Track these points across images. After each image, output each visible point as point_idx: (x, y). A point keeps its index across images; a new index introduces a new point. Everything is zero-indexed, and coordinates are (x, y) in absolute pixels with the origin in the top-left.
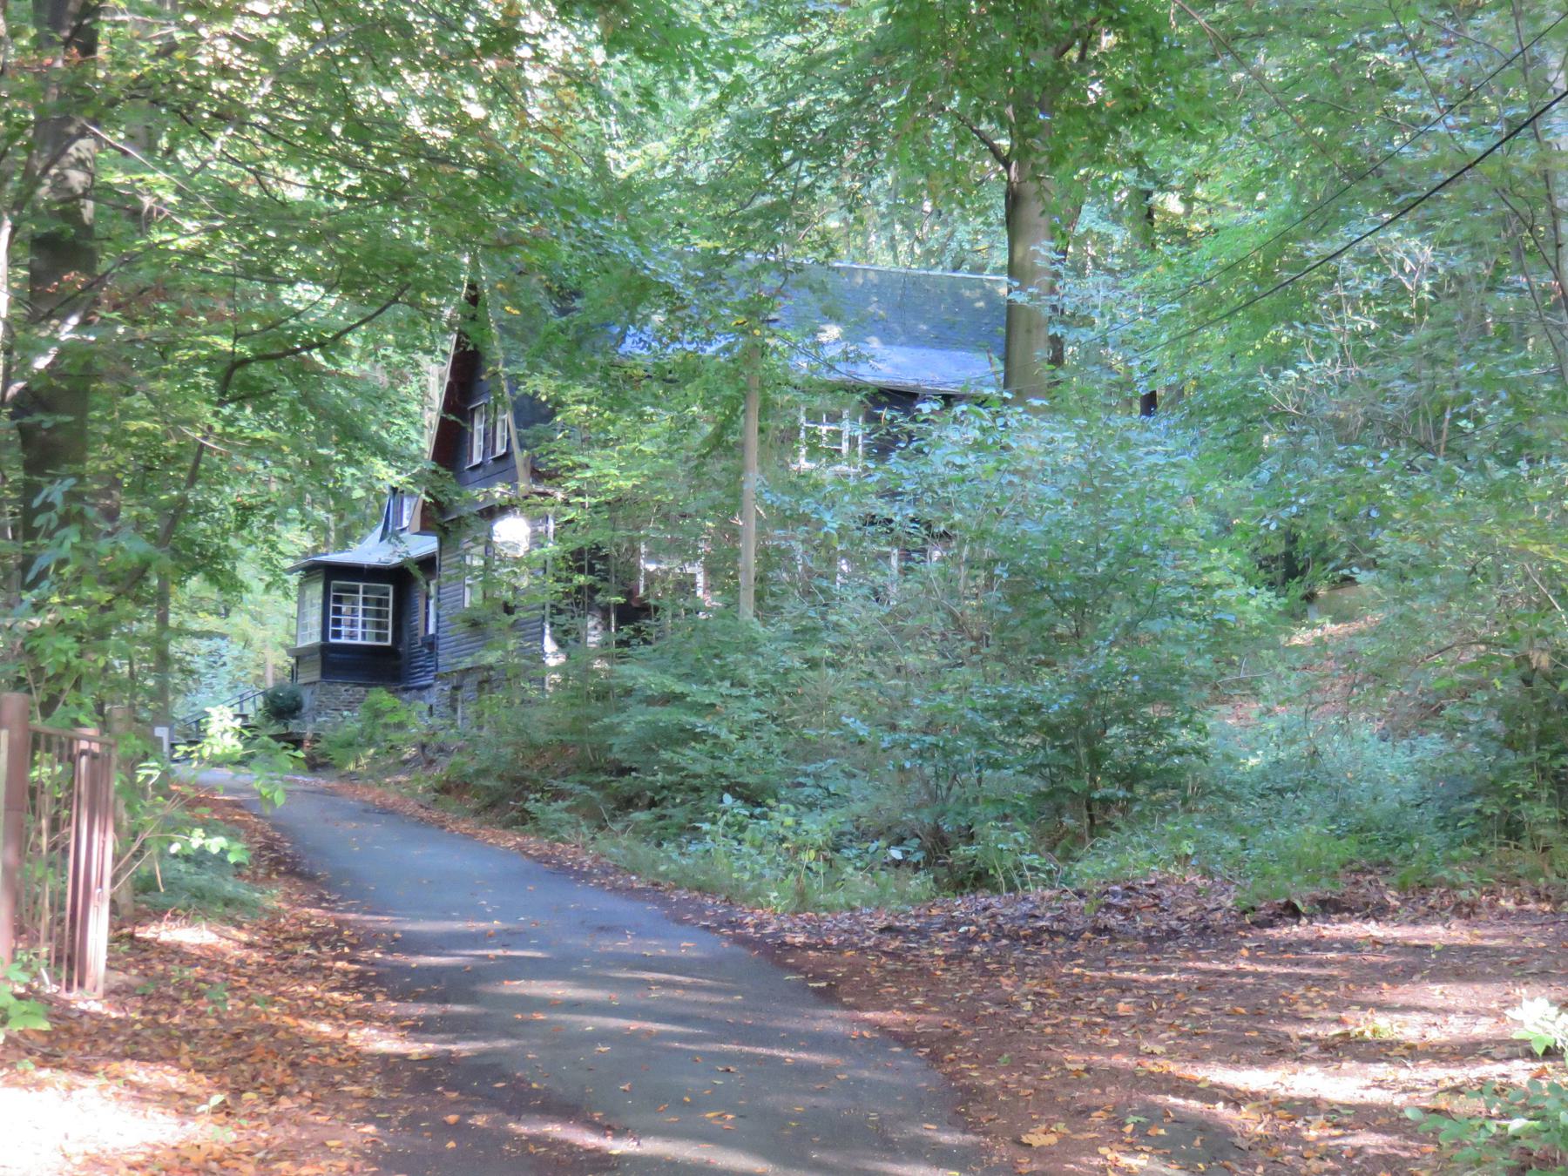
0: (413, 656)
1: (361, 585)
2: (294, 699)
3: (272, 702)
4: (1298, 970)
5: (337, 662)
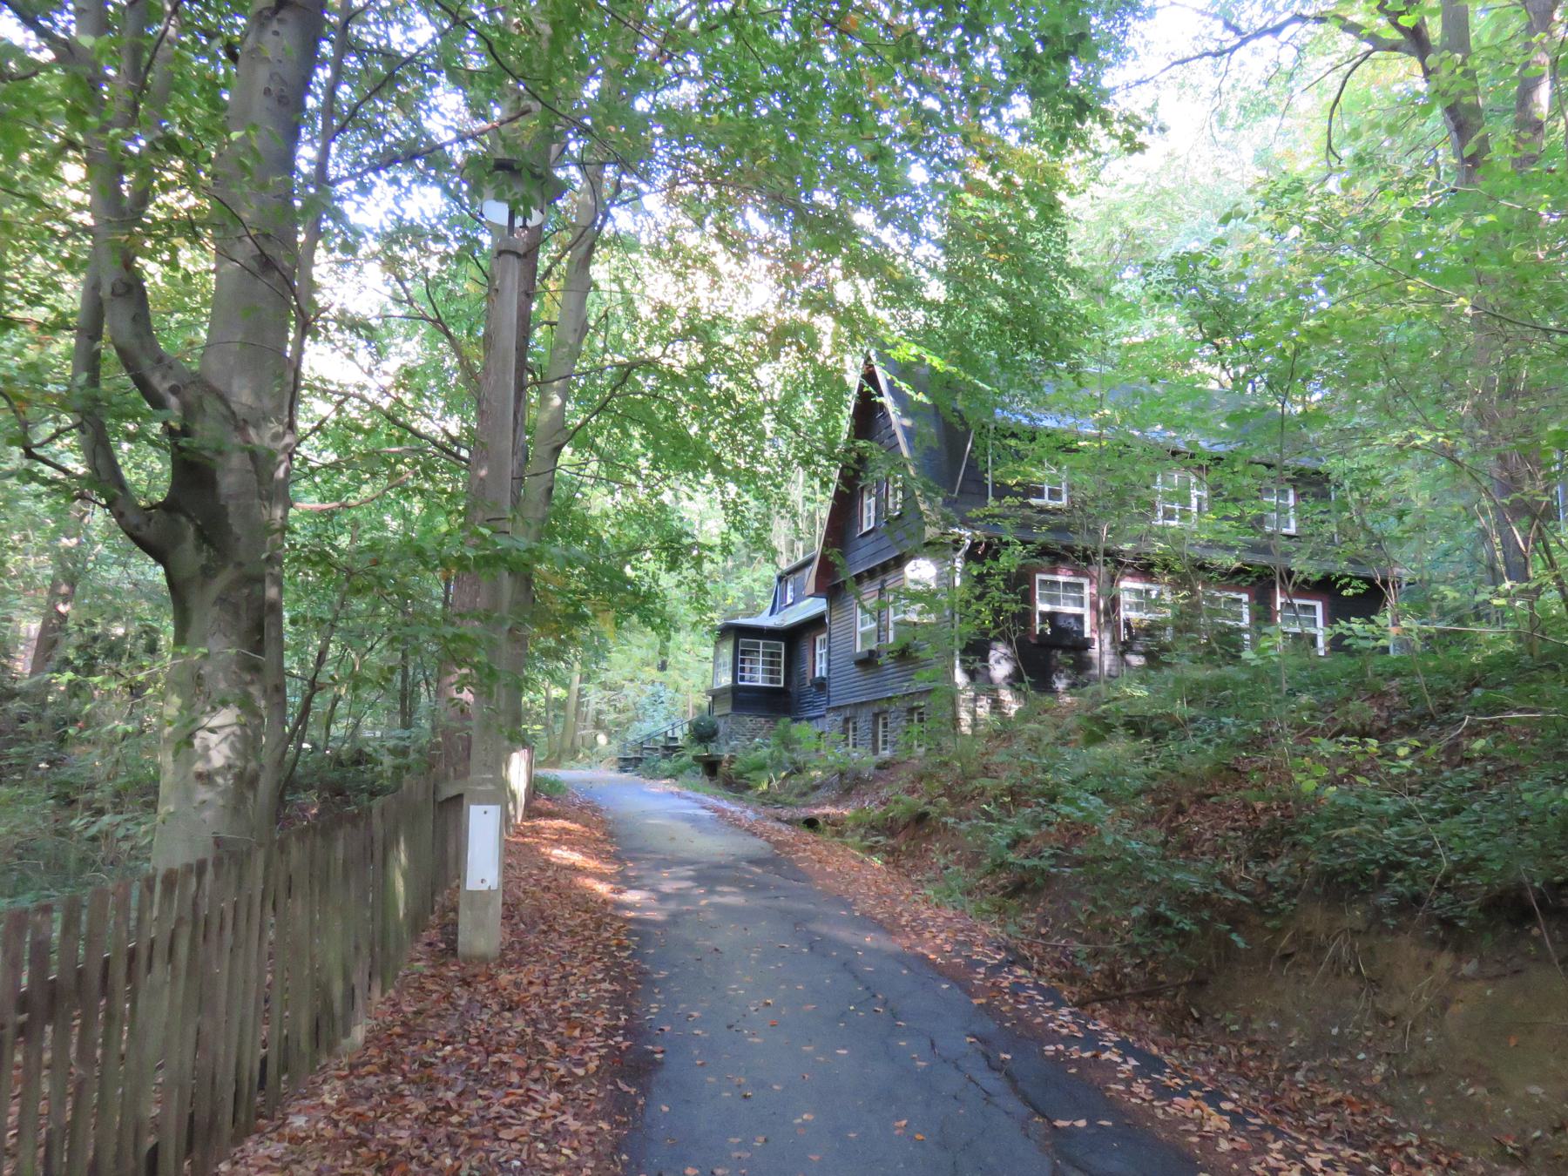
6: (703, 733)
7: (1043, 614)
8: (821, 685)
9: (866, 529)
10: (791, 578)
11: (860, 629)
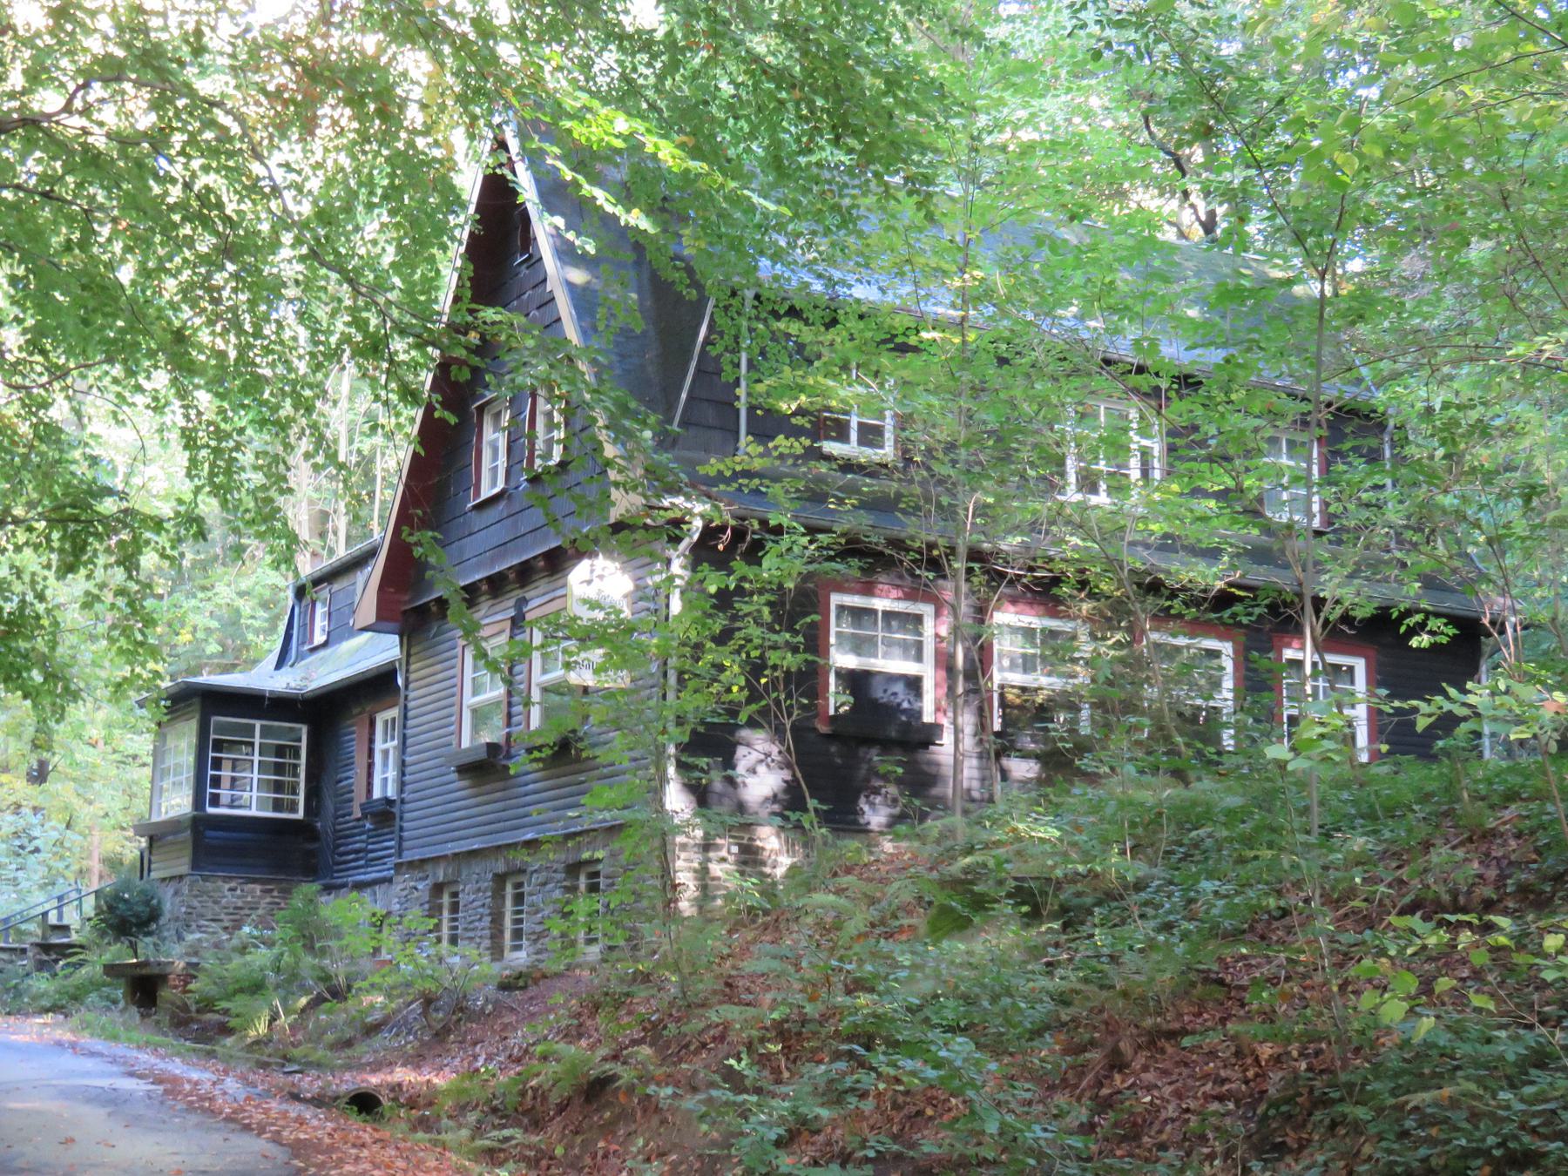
0: (341, 836)
1: (258, 724)
2: (147, 903)
3: (111, 908)
4: (508, 935)
5: (214, 843)
6: (126, 917)
8: (385, 815)
10: (325, 592)
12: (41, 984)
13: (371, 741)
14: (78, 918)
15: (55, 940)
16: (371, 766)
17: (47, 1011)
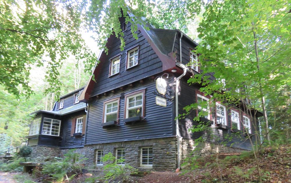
1: (52, 119)
5: (42, 140)
6: (24, 153)
7: (52, 133)
8: (79, 136)
9: (112, 75)
10: (63, 100)
11: (106, 114)
12: (5, 165)
13: (76, 123)
14: (13, 152)
15: (7, 156)
16: (75, 127)
17: (6, 172)
